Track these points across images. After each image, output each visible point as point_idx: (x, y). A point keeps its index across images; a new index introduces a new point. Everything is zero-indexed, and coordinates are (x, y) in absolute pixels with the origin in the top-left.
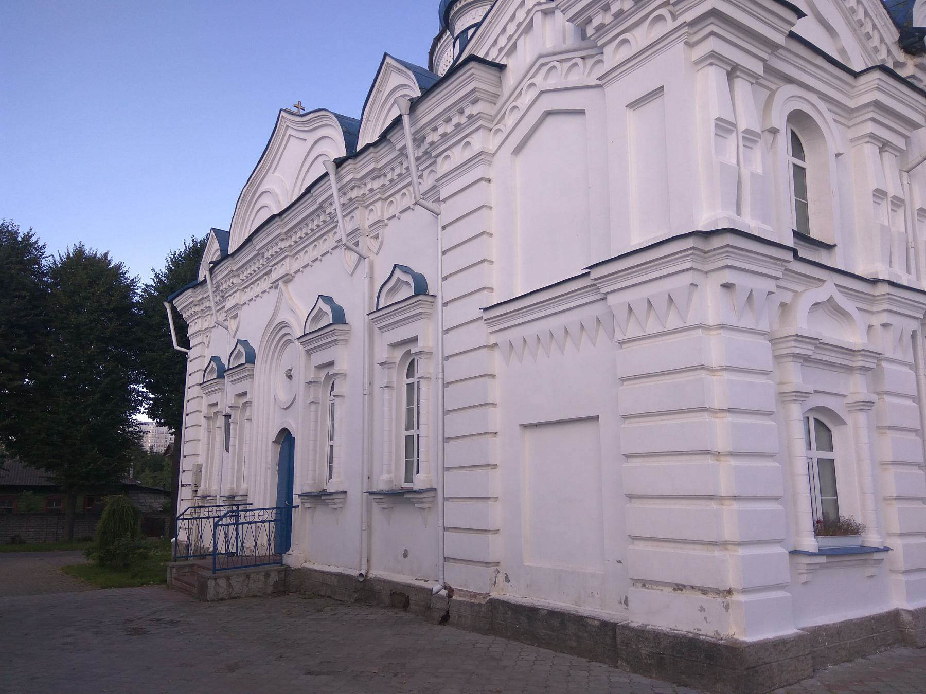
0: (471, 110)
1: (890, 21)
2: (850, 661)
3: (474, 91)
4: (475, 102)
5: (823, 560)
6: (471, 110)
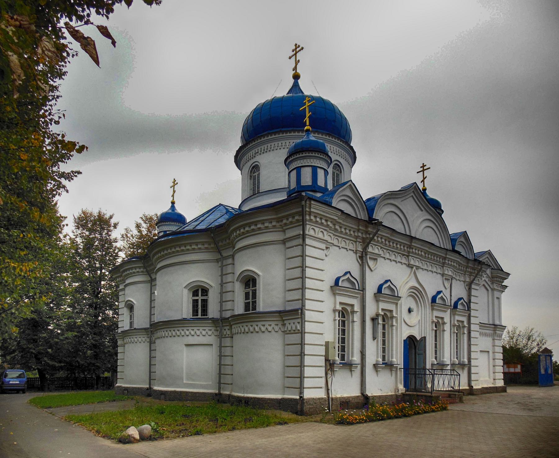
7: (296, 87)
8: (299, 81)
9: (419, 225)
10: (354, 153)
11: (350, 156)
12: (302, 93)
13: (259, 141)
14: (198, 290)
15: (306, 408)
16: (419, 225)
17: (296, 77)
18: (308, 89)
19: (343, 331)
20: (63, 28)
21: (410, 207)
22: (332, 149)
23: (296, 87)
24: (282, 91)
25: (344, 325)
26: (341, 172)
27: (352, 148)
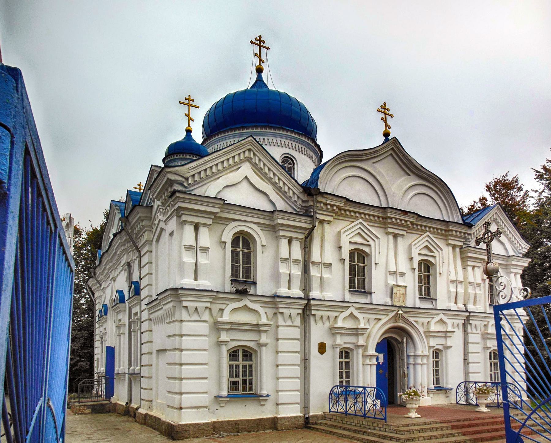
0: (144, 223)
1: (9, 311)
2: (248, 432)
3: (140, 217)
4: (142, 221)
5: (229, 399)
6: (144, 223)
7: (259, 80)
8: (263, 75)
9: (402, 193)
10: (321, 152)
11: (314, 151)
12: (267, 87)
13: (241, 131)
14: (239, 237)
15: (280, 424)
16: (402, 193)
17: (259, 70)
18: (273, 83)
19: (437, 371)
20: (515, 363)
21: (385, 170)
22: (300, 148)
23: (259, 80)
24: (246, 82)
25: (437, 365)
26: (294, 163)
27: (318, 146)
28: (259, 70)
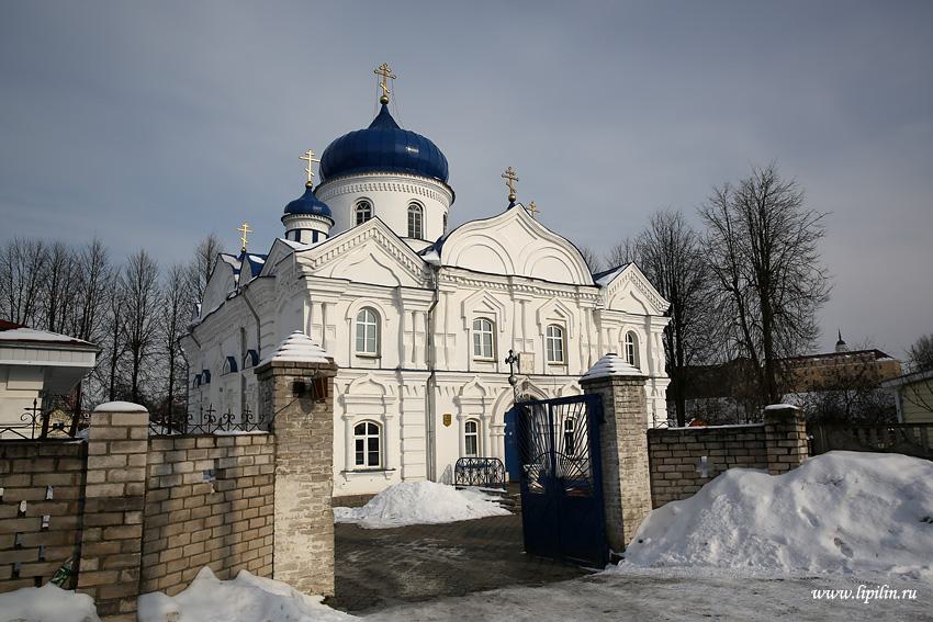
10: (453, 193)
11: (445, 193)
17: (384, 103)
27: (449, 188)
28: (384, 103)
